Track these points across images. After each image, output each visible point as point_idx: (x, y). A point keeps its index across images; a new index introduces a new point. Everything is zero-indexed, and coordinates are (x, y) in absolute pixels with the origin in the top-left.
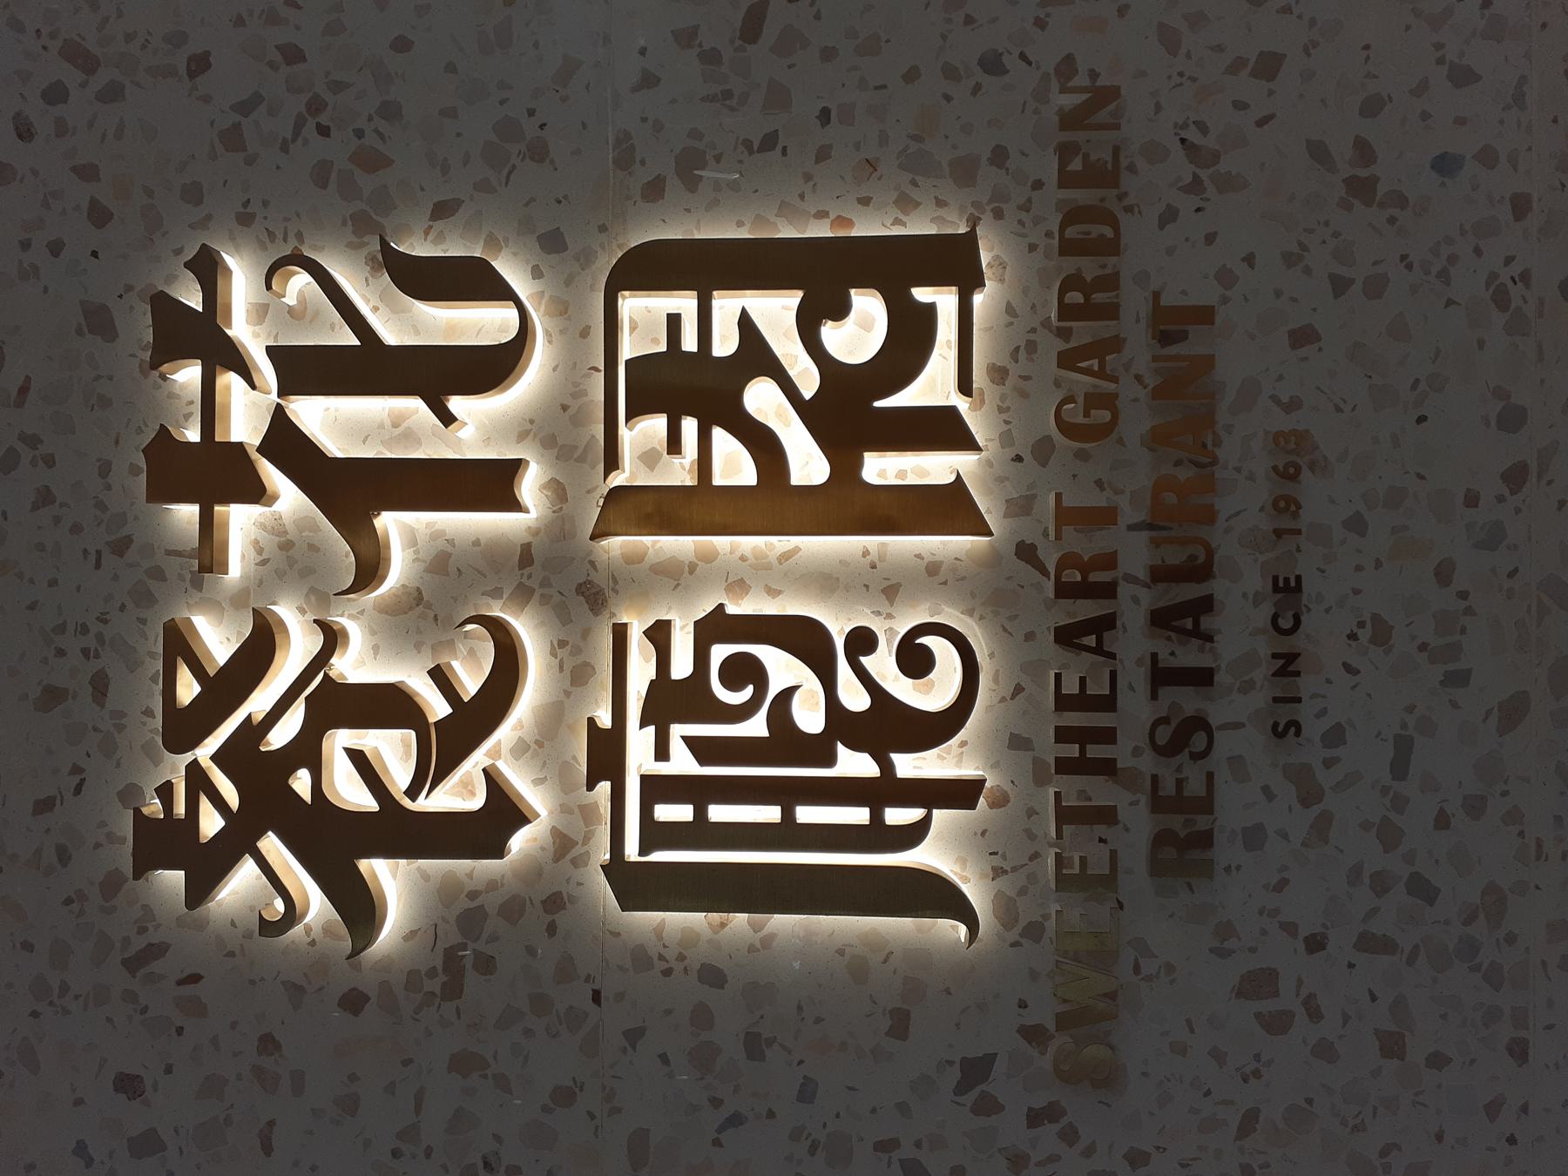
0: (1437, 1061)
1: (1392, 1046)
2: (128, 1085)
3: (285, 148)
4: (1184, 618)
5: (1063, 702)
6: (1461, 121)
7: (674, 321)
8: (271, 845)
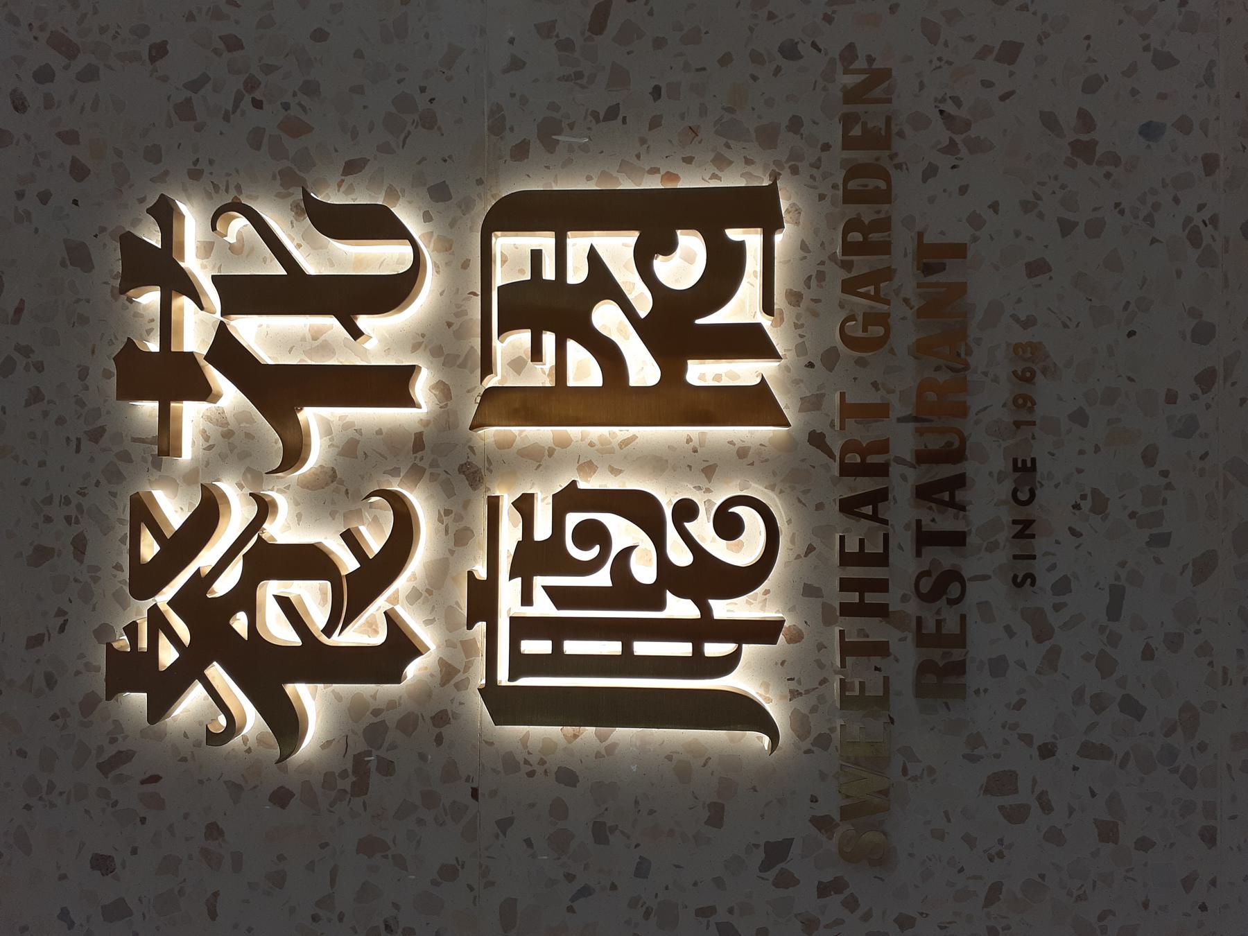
0: (1144, 844)
1: (1108, 833)
2: (102, 864)
3: (227, 118)
4: (943, 492)
5: (846, 559)
6: (1163, 97)
7: (536, 256)
8: (216, 673)
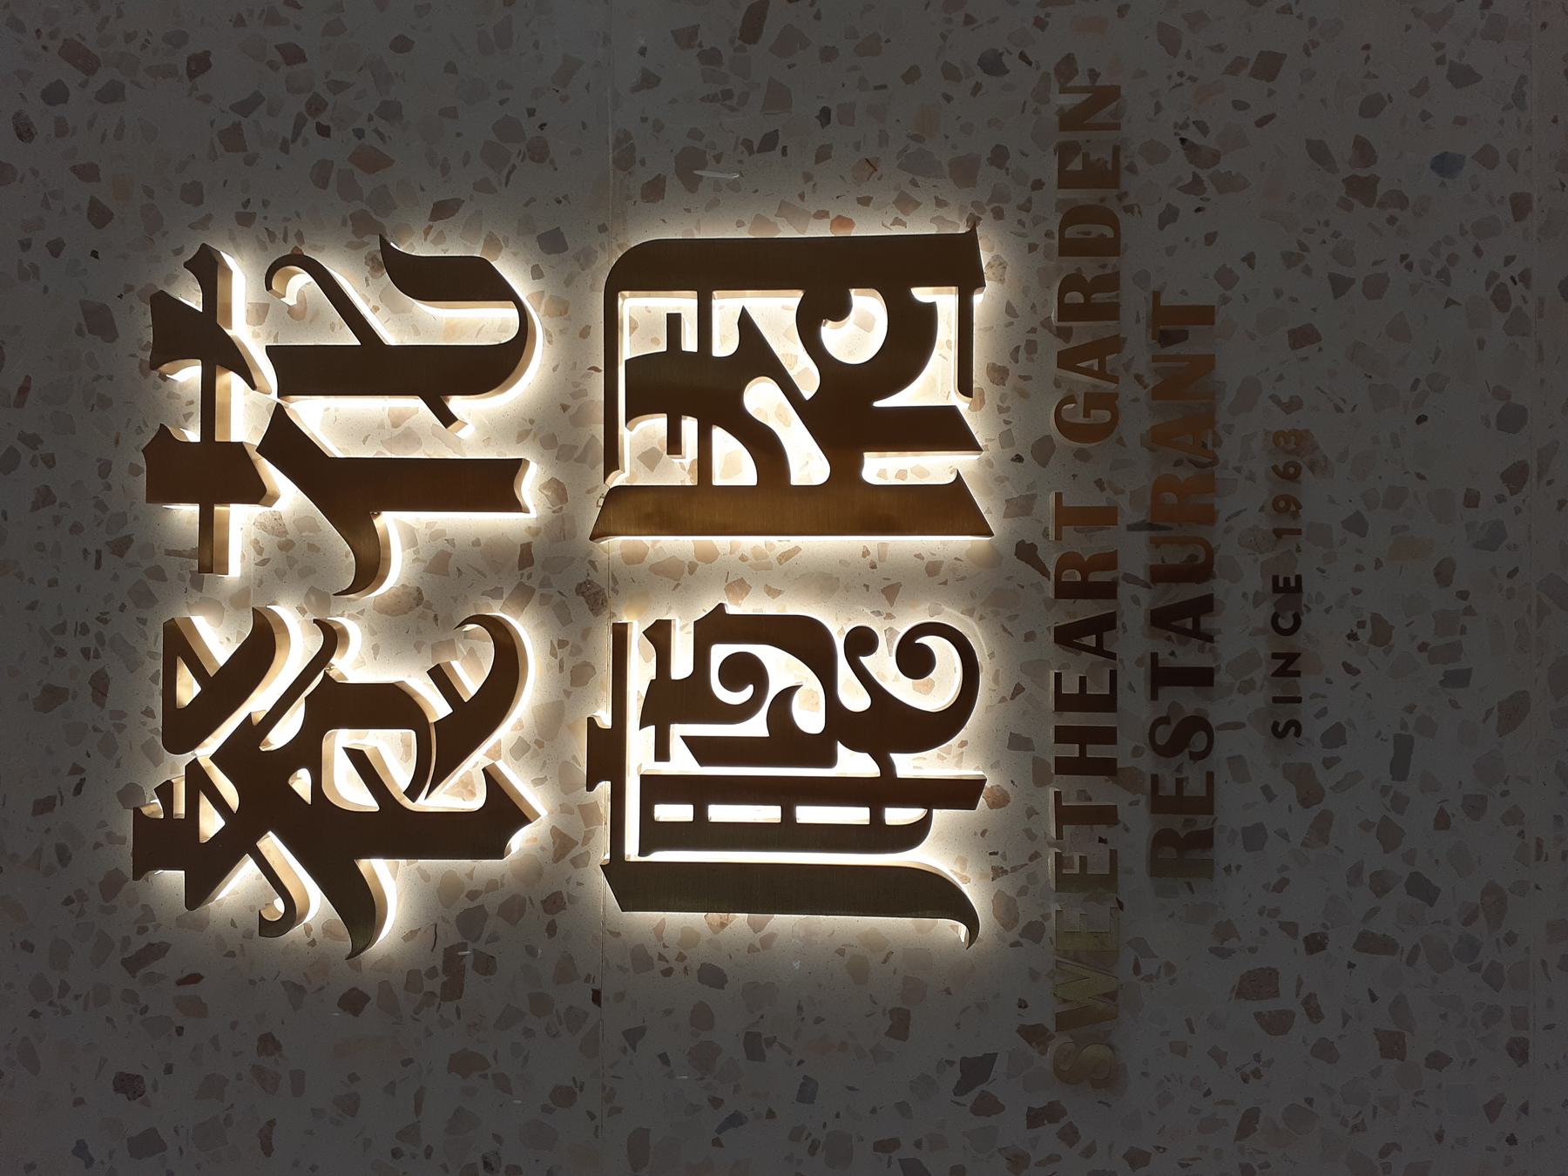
0: (1437, 1061)
1: (1392, 1046)
2: (128, 1085)
3: (285, 148)
4: (1184, 618)
5: (1063, 702)
6: (1461, 121)
7: (674, 321)
8: (271, 845)
